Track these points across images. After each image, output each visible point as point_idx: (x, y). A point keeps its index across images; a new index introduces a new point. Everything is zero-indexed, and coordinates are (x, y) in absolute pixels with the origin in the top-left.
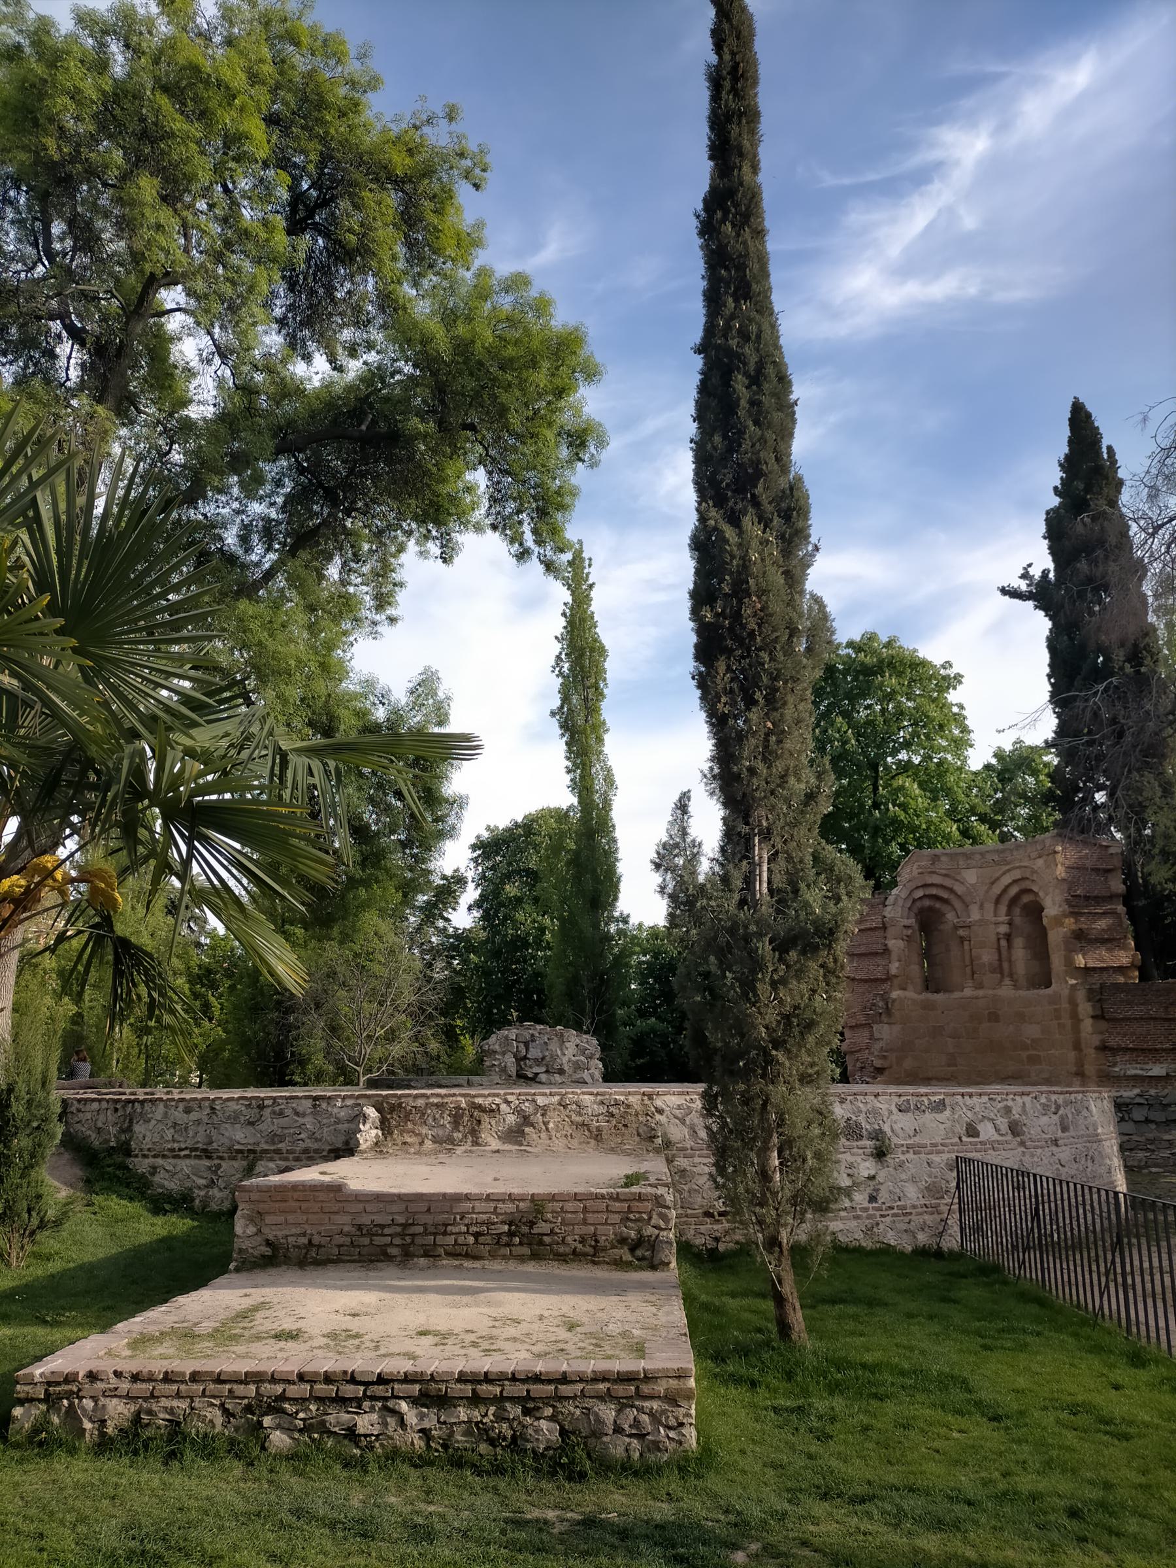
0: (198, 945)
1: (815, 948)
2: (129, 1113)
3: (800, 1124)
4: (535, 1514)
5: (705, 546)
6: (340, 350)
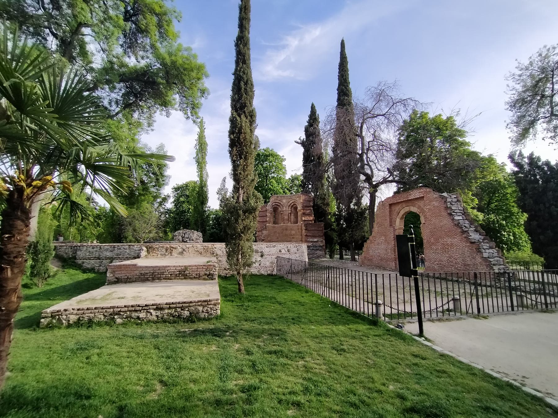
0: (96, 209)
1: (252, 213)
2: (75, 249)
3: (246, 249)
4: (183, 330)
5: (233, 121)
6: (139, 57)
